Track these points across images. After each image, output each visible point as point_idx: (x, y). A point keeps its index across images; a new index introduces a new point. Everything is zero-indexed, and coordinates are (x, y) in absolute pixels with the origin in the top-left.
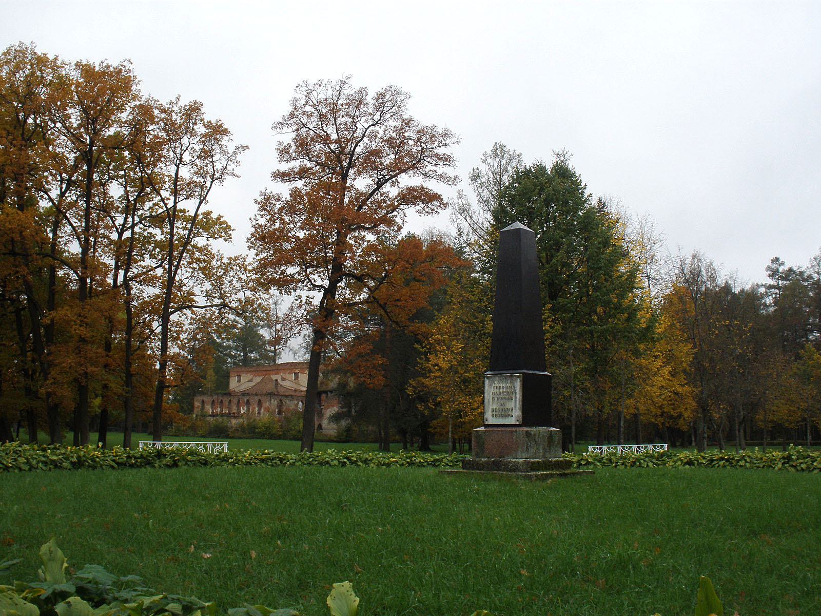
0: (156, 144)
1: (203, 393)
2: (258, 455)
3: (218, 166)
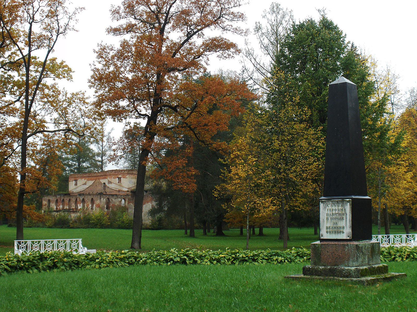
0: (13, 7)
1: (48, 194)
2: (117, 255)
3: (62, 23)
